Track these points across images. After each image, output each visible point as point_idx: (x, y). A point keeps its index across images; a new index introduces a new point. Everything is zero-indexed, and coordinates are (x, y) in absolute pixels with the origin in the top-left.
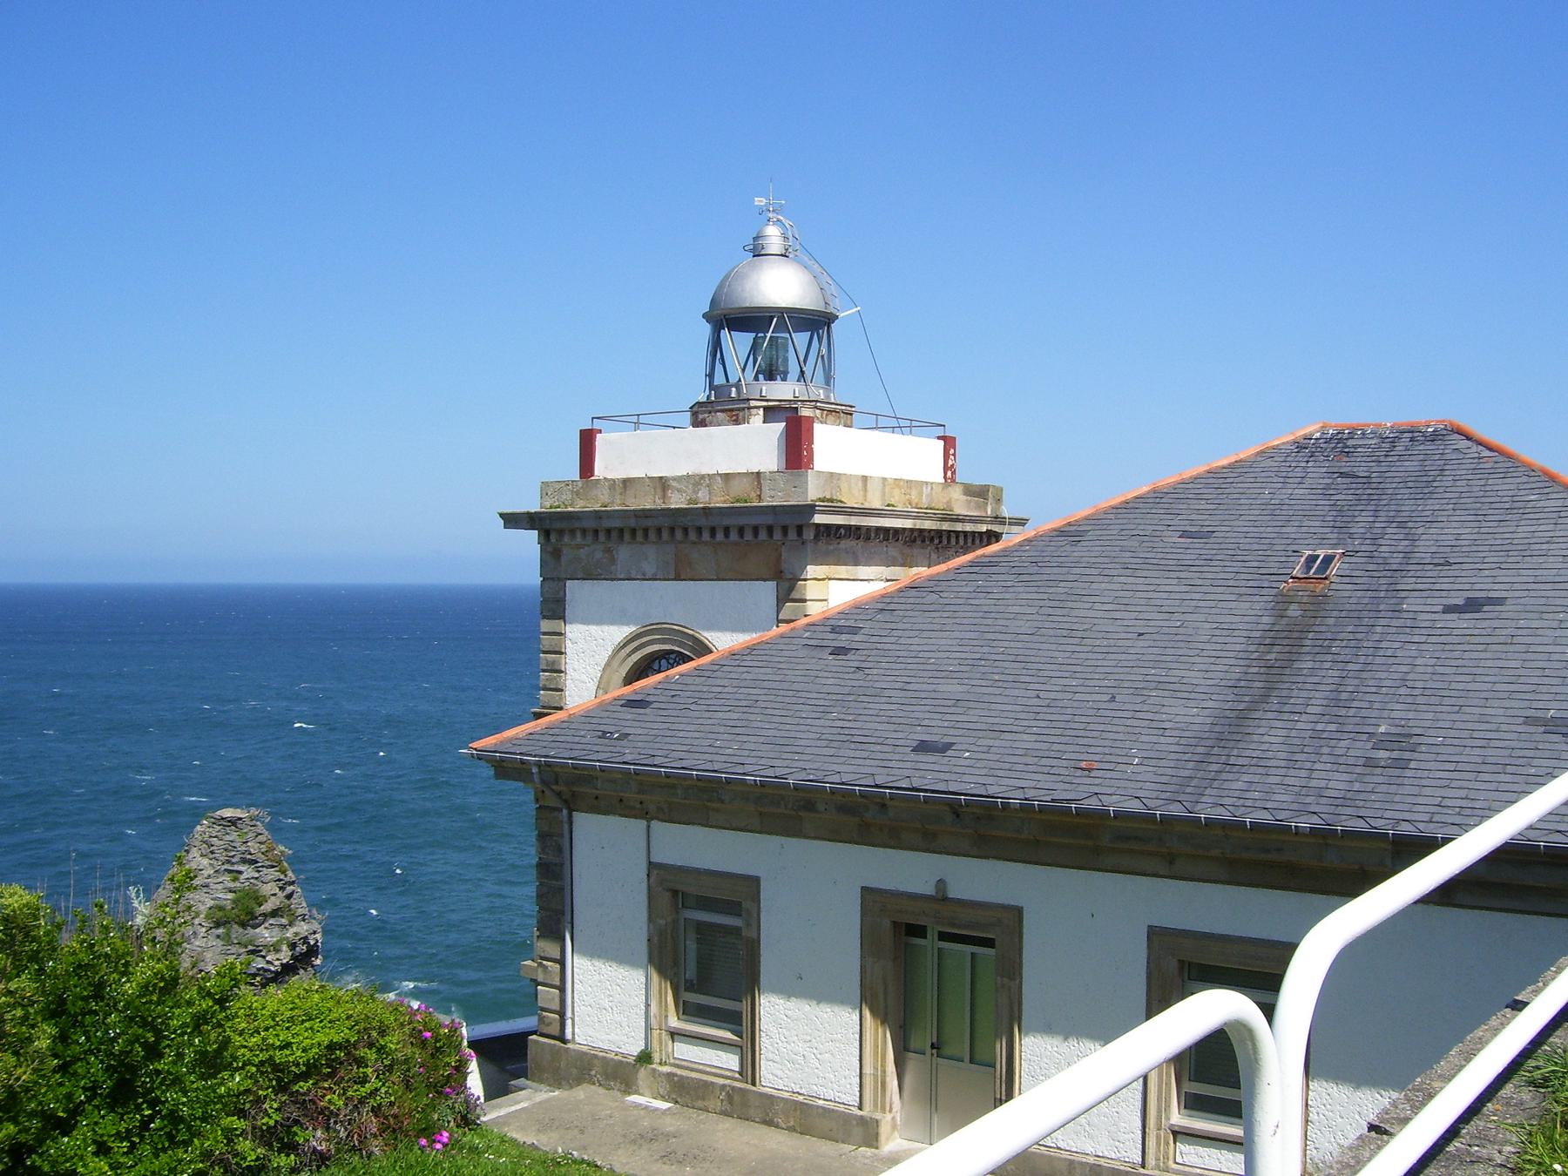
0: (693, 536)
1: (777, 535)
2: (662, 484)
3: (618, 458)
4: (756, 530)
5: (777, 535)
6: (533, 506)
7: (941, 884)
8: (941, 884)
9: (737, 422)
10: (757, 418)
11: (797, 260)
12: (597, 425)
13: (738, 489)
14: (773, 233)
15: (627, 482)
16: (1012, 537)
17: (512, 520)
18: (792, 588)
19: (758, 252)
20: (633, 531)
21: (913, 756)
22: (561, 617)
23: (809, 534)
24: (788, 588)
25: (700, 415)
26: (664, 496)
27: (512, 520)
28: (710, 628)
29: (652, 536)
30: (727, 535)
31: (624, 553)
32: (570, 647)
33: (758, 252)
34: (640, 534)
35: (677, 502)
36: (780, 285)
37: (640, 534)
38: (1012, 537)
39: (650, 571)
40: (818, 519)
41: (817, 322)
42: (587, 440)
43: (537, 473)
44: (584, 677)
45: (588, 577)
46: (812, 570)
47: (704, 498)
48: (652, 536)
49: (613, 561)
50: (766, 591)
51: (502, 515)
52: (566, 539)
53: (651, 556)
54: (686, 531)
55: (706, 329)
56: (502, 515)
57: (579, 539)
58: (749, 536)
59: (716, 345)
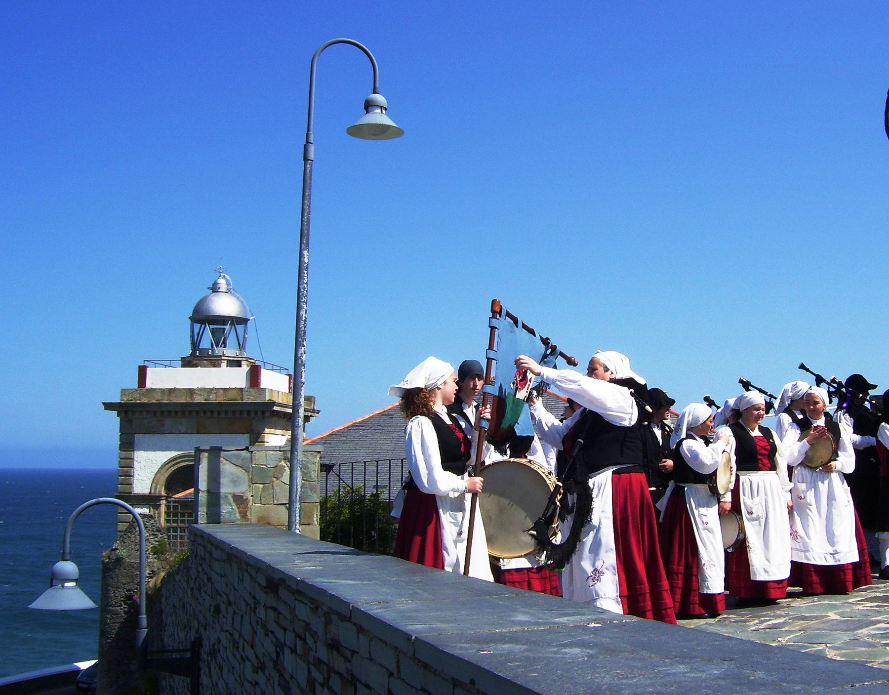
0: (209, 415)
1: (252, 415)
2: (191, 392)
3: (160, 379)
4: (234, 412)
5: (252, 415)
6: (117, 399)
9: (215, 366)
10: (224, 365)
12: (146, 364)
13: (230, 395)
14: (222, 282)
15: (171, 391)
16: (266, 444)
17: (108, 406)
18: (258, 437)
19: (215, 289)
20: (176, 412)
21: (316, 498)
23: (268, 414)
24: (256, 438)
25: (187, 363)
26: (192, 397)
27: (108, 406)
29: (187, 414)
31: (168, 422)
32: (136, 465)
33: (215, 289)
35: (198, 399)
36: (225, 305)
38: (266, 444)
40: (275, 408)
41: (241, 321)
42: (142, 372)
43: (119, 384)
44: (144, 478)
45: (148, 432)
46: (267, 430)
47: (213, 398)
48: (187, 414)
49: (163, 425)
50: (244, 439)
51: (104, 403)
52: (137, 415)
56: (104, 403)
57: (145, 415)
58: (238, 415)
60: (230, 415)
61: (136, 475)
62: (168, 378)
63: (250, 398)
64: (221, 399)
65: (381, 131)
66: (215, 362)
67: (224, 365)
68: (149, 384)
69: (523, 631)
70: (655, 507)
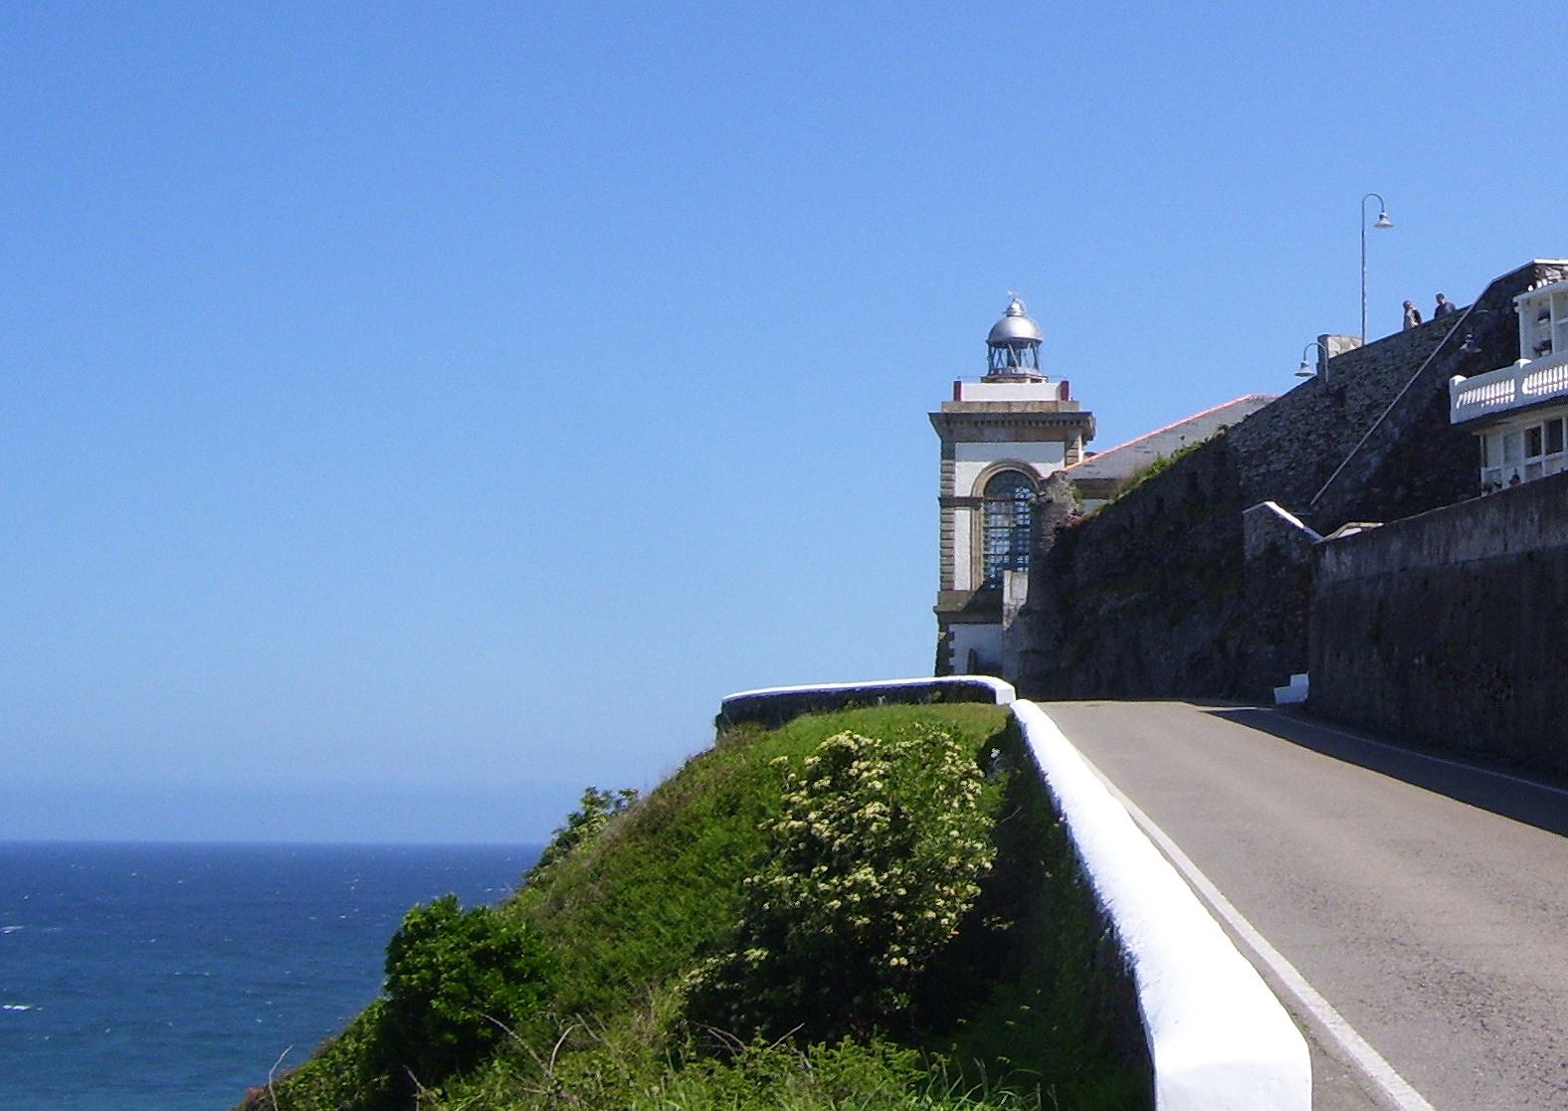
2: (1009, 404)
4: (1065, 422)
7: (1562, 469)
8: (1562, 469)
11: (1026, 318)
12: (961, 380)
14: (1016, 306)
19: (1010, 313)
20: (990, 422)
22: (953, 458)
28: (1032, 461)
30: (1037, 424)
33: (1010, 313)
34: (1000, 424)
36: (1021, 328)
37: (1000, 424)
39: (1001, 438)
42: (957, 386)
43: (939, 399)
47: (1029, 410)
51: (930, 414)
52: (958, 425)
53: (1002, 433)
54: (1030, 422)
55: (987, 346)
56: (930, 414)
59: (991, 356)
60: (1048, 425)
61: (957, 480)
62: (979, 393)
63: (955, 409)
64: (1001, 410)
65: (1386, 225)
66: (1020, 378)
67: (1029, 381)
68: (963, 398)
69: (1367, 738)
70: (660, 1087)
